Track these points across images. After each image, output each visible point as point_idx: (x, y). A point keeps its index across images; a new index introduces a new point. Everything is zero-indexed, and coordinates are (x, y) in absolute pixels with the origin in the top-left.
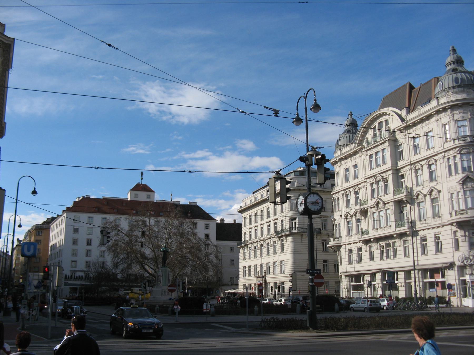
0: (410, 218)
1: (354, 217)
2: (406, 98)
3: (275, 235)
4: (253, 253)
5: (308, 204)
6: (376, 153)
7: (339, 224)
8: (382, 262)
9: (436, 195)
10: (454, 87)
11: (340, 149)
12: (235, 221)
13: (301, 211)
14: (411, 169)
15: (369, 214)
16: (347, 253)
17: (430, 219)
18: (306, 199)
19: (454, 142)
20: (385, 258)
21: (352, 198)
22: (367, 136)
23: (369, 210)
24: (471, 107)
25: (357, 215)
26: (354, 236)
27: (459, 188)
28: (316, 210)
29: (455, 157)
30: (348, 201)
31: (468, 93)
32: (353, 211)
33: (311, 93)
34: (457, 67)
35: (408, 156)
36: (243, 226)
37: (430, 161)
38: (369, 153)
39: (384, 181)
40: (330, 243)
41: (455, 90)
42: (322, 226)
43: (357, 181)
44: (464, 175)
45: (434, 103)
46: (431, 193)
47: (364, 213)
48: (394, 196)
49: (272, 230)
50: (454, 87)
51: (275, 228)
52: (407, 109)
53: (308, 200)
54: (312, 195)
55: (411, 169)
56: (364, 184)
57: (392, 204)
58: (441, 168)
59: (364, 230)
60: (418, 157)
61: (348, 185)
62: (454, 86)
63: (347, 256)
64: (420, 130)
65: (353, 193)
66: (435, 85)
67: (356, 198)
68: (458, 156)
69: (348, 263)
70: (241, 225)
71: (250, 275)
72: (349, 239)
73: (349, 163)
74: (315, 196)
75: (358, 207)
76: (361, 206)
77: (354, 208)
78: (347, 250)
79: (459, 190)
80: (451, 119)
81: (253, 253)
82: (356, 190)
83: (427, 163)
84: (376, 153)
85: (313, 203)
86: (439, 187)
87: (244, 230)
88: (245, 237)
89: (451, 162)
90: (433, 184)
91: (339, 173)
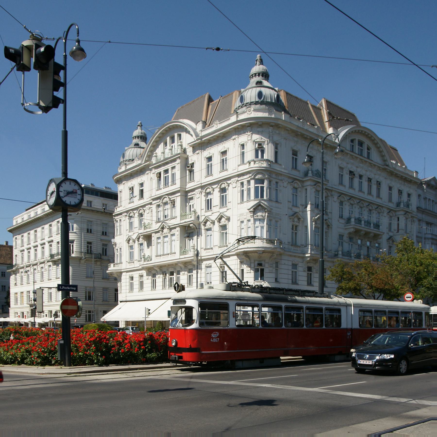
0: (196, 245)
1: (136, 241)
2: (202, 112)
3: (49, 258)
4: (25, 278)
5: (62, 194)
6: (166, 171)
7: (121, 249)
8: (164, 291)
9: (225, 222)
10: (256, 103)
11: (126, 164)
12: (7, 243)
13: (51, 204)
14: (201, 192)
15: (153, 239)
16: (128, 280)
17: (217, 247)
18: (58, 186)
19: (249, 165)
20: (167, 286)
21: (136, 220)
22: (157, 151)
23: (153, 235)
24: (271, 128)
25: (141, 239)
26: (135, 262)
27: (249, 216)
28: (73, 203)
29: (249, 182)
30: (131, 224)
31: (270, 112)
32: (136, 235)
33: (72, 35)
34: (262, 80)
35: (200, 177)
36: (14, 248)
37: (222, 186)
38: (158, 170)
39: (171, 203)
40: (109, 269)
41: (258, 106)
42: (103, 251)
43: (142, 202)
44: (256, 202)
45: (233, 119)
46: (220, 220)
47: (148, 238)
48: (181, 220)
49: (47, 254)
50: (256, 103)
51: (51, 250)
52: (203, 123)
53: (61, 189)
54: (68, 183)
55: (201, 192)
56: (149, 206)
57: (178, 229)
58: (233, 193)
59: (146, 257)
60: (210, 179)
61: (132, 206)
62: (256, 102)
63: (128, 284)
64: (214, 151)
65: (137, 215)
66: (235, 99)
67: (141, 221)
68: (252, 182)
69: (128, 291)
70: (11, 247)
71: (22, 303)
72: (130, 265)
73: (135, 182)
74: (73, 184)
75: (142, 231)
76: (145, 229)
77: (137, 231)
78: (128, 277)
79: (249, 218)
80: (249, 138)
81: (25, 278)
82: (141, 212)
83: (219, 187)
84: (166, 171)
85: (69, 193)
86: (228, 214)
87: (16, 252)
88: (16, 259)
89: (245, 187)
90: (222, 210)
91: (123, 192)
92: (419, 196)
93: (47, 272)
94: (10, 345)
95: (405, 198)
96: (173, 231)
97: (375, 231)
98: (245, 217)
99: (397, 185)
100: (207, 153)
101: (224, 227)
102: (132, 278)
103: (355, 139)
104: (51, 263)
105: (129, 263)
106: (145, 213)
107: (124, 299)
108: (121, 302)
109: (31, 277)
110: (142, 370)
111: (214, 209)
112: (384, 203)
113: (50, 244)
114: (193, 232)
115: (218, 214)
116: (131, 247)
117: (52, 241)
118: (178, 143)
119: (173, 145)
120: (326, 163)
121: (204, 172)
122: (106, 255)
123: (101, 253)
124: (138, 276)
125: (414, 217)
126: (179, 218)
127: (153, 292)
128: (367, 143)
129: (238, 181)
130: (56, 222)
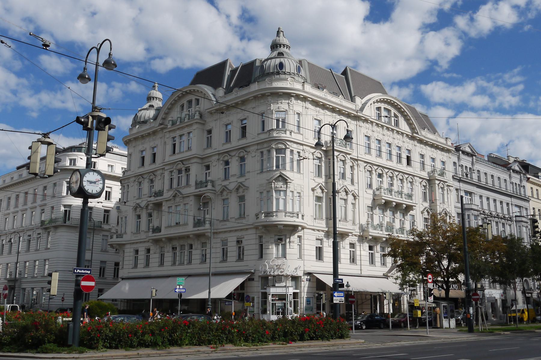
21: (146, 186)
38: (173, 135)
55: (218, 159)
78: (132, 250)
92: (455, 163)
93: (35, 241)
94: (515, 321)
95: (439, 166)
96: (186, 200)
97: (408, 202)
98: (265, 188)
99: (429, 152)
100: (225, 119)
101: (242, 199)
102: (137, 252)
103: (380, 107)
104: (40, 231)
105: (134, 234)
106: (157, 180)
107: (125, 275)
108: (123, 279)
109: (15, 247)
110: (266, 140)
111: (232, 179)
112: (416, 172)
113: (42, 208)
114: (208, 202)
115: (236, 183)
116: (139, 217)
117: (45, 205)
118: (195, 108)
119: (190, 109)
120: (351, 131)
121: (223, 140)
122: (107, 222)
123: (102, 220)
124: (143, 249)
125: (450, 186)
126: (194, 188)
127: (161, 268)
128: (393, 111)
129: (257, 149)
130: (52, 185)
